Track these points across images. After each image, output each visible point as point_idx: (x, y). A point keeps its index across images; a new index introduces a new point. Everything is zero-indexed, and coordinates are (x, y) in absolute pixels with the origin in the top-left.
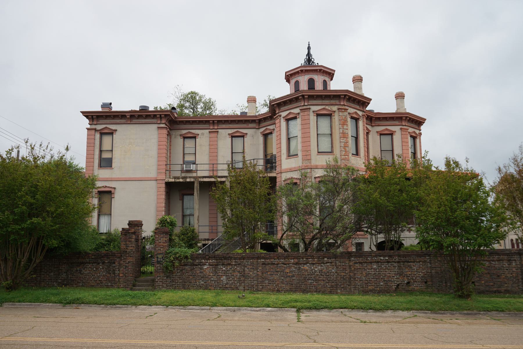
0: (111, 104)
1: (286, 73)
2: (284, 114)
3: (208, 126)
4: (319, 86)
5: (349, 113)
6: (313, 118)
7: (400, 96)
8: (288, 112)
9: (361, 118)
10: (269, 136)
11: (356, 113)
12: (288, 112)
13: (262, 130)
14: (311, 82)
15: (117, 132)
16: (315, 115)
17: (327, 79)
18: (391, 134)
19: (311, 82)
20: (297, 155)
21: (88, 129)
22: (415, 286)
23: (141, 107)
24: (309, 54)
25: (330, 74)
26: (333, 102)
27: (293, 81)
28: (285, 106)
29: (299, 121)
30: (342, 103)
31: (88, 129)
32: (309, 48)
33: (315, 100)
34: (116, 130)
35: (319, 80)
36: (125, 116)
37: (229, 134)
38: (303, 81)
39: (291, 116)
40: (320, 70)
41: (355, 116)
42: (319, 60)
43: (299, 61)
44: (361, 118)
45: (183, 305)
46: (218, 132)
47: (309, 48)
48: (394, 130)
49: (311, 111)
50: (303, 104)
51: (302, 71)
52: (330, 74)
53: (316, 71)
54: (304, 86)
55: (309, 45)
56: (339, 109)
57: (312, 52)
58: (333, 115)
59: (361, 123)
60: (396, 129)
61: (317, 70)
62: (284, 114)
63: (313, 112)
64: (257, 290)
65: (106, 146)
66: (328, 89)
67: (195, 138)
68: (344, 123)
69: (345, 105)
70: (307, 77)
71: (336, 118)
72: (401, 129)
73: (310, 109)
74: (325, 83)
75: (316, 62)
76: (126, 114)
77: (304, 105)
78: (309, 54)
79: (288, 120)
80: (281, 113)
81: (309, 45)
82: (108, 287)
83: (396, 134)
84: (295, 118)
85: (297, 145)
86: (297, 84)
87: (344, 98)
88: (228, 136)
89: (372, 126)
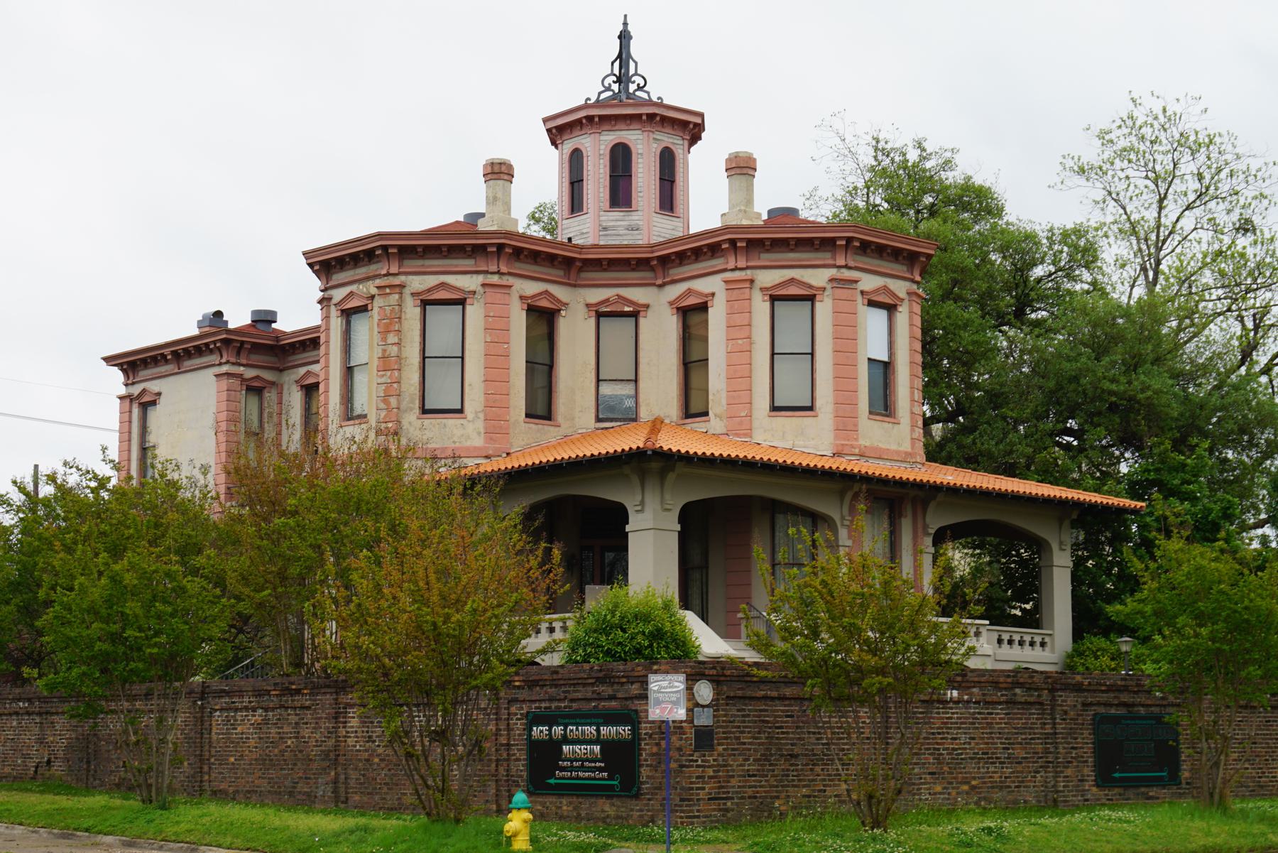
5: (862, 292)
8: (432, 281)
9: (906, 303)
11: (885, 289)
12: (432, 281)
16: (767, 298)
21: (121, 398)
27: (568, 146)
28: (697, 260)
30: (841, 262)
31: (121, 398)
32: (624, 37)
33: (792, 251)
40: (651, 117)
41: (544, 303)
43: (585, 84)
44: (906, 303)
47: (624, 37)
51: (590, 119)
55: (625, 24)
57: (635, 49)
58: (818, 298)
61: (640, 116)
64: (951, 812)
69: (850, 268)
70: (609, 138)
78: (623, 57)
81: (625, 24)
84: (363, 309)
87: (847, 246)
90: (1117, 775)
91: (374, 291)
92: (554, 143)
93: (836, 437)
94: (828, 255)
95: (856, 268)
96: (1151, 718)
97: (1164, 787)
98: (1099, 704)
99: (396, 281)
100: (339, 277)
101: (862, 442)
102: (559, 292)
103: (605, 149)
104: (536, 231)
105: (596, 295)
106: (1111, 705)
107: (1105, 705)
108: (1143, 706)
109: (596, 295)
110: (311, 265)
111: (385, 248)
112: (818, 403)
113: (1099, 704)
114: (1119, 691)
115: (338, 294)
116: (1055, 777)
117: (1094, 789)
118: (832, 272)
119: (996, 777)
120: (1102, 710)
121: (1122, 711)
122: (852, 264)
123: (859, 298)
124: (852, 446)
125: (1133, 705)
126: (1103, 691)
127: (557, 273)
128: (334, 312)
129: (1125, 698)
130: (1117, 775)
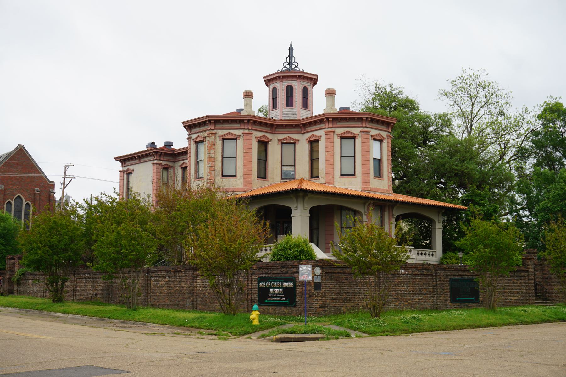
0: (153, 143)
3: (360, 123)
10: (130, 175)
13: (308, 135)
15: (299, 142)
21: (120, 171)
22: (99, 297)
23: (165, 142)
26: (202, 129)
27: (272, 86)
31: (120, 171)
32: (291, 49)
34: (299, 140)
36: (135, 157)
40: (300, 76)
42: (305, 65)
43: (277, 65)
45: (102, 318)
46: (334, 132)
47: (291, 49)
48: (319, 135)
49: (217, 135)
51: (279, 77)
55: (291, 45)
57: (294, 53)
65: (288, 160)
68: (212, 147)
70: (286, 83)
76: (136, 156)
78: (290, 56)
81: (291, 45)
82: (320, 316)
85: (203, 171)
91: (206, 135)
92: (267, 85)
93: (362, 185)
101: (372, 186)
103: (284, 87)
106: (456, 275)
110: (184, 127)
112: (356, 173)
115: (194, 136)
121: (459, 277)
128: (192, 142)
129: (460, 273)
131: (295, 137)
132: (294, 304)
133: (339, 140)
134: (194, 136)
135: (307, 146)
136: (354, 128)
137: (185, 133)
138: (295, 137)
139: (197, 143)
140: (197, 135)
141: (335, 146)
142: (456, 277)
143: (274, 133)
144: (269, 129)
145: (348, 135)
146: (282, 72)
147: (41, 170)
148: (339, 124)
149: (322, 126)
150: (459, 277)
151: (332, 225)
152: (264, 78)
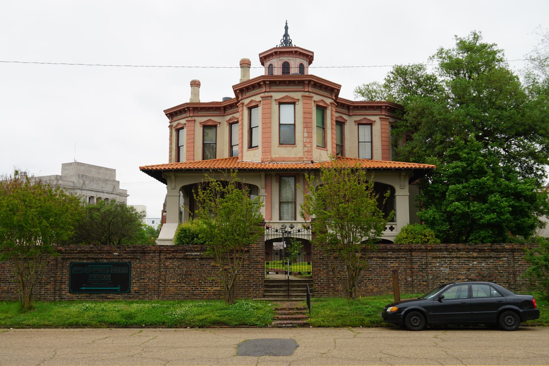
1: (260, 55)
2: (246, 101)
4: (294, 70)
5: (314, 101)
6: (275, 106)
7: (195, 84)
9: (330, 107)
13: (228, 118)
14: (286, 67)
17: (305, 63)
18: (371, 124)
19: (286, 67)
20: (257, 146)
24: (286, 35)
25: (309, 57)
27: (267, 64)
29: (260, 108)
30: (306, 90)
32: (286, 28)
35: (294, 63)
37: (200, 123)
38: (277, 63)
39: (253, 104)
40: (296, 52)
42: (297, 42)
43: (276, 42)
44: (330, 107)
46: (195, 121)
47: (286, 28)
50: (264, 91)
51: (276, 53)
52: (309, 57)
53: (290, 53)
54: (278, 72)
55: (286, 23)
56: (302, 96)
57: (289, 32)
59: (328, 112)
60: (376, 118)
62: (246, 101)
63: (275, 100)
66: (306, 74)
67: (215, 126)
69: (310, 92)
71: (299, 106)
72: (380, 118)
73: (271, 97)
74: (302, 67)
75: (294, 44)
77: (266, 92)
78: (286, 35)
79: (250, 109)
80: (243, 101)
81: (286, 23)
83: (376, 124)
84: (257, 106)
86: (271, 67)
88: (354, 124)
89: (349, 115)
90: (83, 288)
91: (185, 122)
92: (263, 64)
93: (262, 156)
94: (302, 87)
95: (312, 92)
96: (111, 264)
97: (118, 294)
98: (73, 258)
99: (193, 118)
100: (175, 118)
101: (274, 156)
102: (345, 117)
103: (281, 63)
104: (361, 99)
105: (358, 118)
106: (84, 259)
107: (80, 259)
108: (106, 259)
109: (358, 118)
110: (166, 115)
111: (188, 108)
112: (297, 143)
113: (73, 258)
114: (87, 253)
115: (175, 124)
116: (40, 289)
117: (69, 294)
118: (302, 93)
119: (5, 288)
120: (74, 261)
121: (93, 261)
122: (310, 90)
123: (313, 103)
124: (267, 158)
125: (97, 259)
126: (76, 253)
127: (345, 111)
128: (174, 130)
129: (92, 256)
130: (83, 288)
131: (216, 119)
132: (128, 291)
133: (201, 128)
134: (175, 124)
135: (227, 128)
136: (328, 99)
137: (167, 121)
138: (216, 119)
139: (178, 131)
140: (177, 122)
141: (272, 122)
142: (85, 261)
143: (224, 116)
144: (329, 94)
145: (210, 123)
146: (279, 48)
147: (107, 169)
148: (200, 113)
149: (184, 115)
150: (93, 261)
151: (371, 176)
152: (260, 55)
